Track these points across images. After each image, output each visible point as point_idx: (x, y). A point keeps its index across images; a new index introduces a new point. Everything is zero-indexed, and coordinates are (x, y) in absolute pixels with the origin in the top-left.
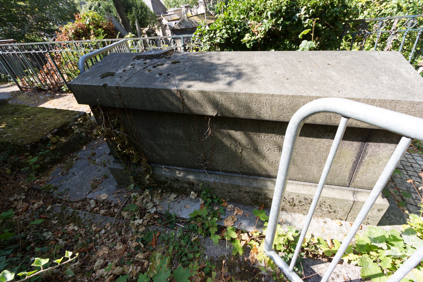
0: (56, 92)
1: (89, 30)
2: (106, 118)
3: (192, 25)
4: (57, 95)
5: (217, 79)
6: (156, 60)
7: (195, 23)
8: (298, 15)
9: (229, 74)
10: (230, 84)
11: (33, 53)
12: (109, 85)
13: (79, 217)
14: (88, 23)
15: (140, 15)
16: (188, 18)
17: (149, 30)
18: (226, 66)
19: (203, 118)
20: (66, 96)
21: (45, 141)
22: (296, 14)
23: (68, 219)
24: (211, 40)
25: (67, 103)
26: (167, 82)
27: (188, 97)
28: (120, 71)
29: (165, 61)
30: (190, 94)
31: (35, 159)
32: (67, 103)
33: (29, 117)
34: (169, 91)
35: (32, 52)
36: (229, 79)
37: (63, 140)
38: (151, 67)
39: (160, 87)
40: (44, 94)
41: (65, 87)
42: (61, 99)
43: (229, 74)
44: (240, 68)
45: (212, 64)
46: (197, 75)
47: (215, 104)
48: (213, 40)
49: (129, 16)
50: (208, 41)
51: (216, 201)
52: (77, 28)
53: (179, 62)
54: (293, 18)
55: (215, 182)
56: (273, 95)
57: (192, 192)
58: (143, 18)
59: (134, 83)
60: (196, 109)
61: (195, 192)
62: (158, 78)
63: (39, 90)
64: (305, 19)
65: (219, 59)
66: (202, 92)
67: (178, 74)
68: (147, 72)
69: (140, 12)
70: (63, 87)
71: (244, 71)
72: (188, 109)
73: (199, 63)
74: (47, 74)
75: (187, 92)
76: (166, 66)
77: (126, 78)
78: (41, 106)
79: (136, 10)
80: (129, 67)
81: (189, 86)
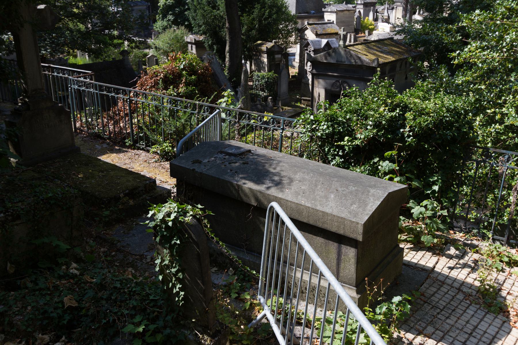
0: (115, 143)
1: (180, 75)
2: (186, 191)
3: (350, 61)
4: (117, 148)
5: (263, 183)
6: (233, 158)
7: (356, 58)
8: (402, 130)
9: (273, 181)
10: (268, 188)
11: (112, 96)
12: (196, 170)
13: (137, 265)
14: (182, 67)
15: (266, 19)
16: (346, 47)
17: (273, 46)
18: (276, 175)
19: (250, 205)
20: (127, 151)
21: (117, 199)
22: (401, 129)
23: (128, 264)
24: (313, 131)
25: (127, 161)
26: (233, 177)
27: (242, 190)
28: (206, 161)
29: (239, 160)
30: (243, 188)
31: (107, 213)
32: (127, 161)
33: (102, 172)
34: (232, 184)
35: (110, 95)
36: (270, 185)
37: (131, 202)
38: (227, 163)
39: (227, 179)
40: (102, 143)
41: (130, 140)
42: (121, 155)
43: (273, 181)
44: (283, 179)
45: (268, 172)
46: (254, 177)
47: (257, 199)
48: (315, 132)
49: (245, 19)
50: (309, 131)
51: (247, 279)
52: (168, 72)
53: (248, 164)
54: (398, 132)
55: (249, 261)
56: (287, 200)
57: (231, 269)
58: (269, 23)
59: (212, 172)
60: (244, 198)
61: (233, 269)
62: (228, 173)
63: (97, 136)
64: (409, 136)
65: (275, 169)
66: (250, 189)
67: (242, 174)
68: (223, 166)
69: (267, 14)
70: (127, 141)
71: (283, 182)
72: (241, 198)
73: (261, 168)
74: (112, 118)
75: (242, 187)
76: (237, 164)
77: (208, 167)
78: (99, 158)
79: (261, 9)
80: (213, 159)
81: (244, 184)
